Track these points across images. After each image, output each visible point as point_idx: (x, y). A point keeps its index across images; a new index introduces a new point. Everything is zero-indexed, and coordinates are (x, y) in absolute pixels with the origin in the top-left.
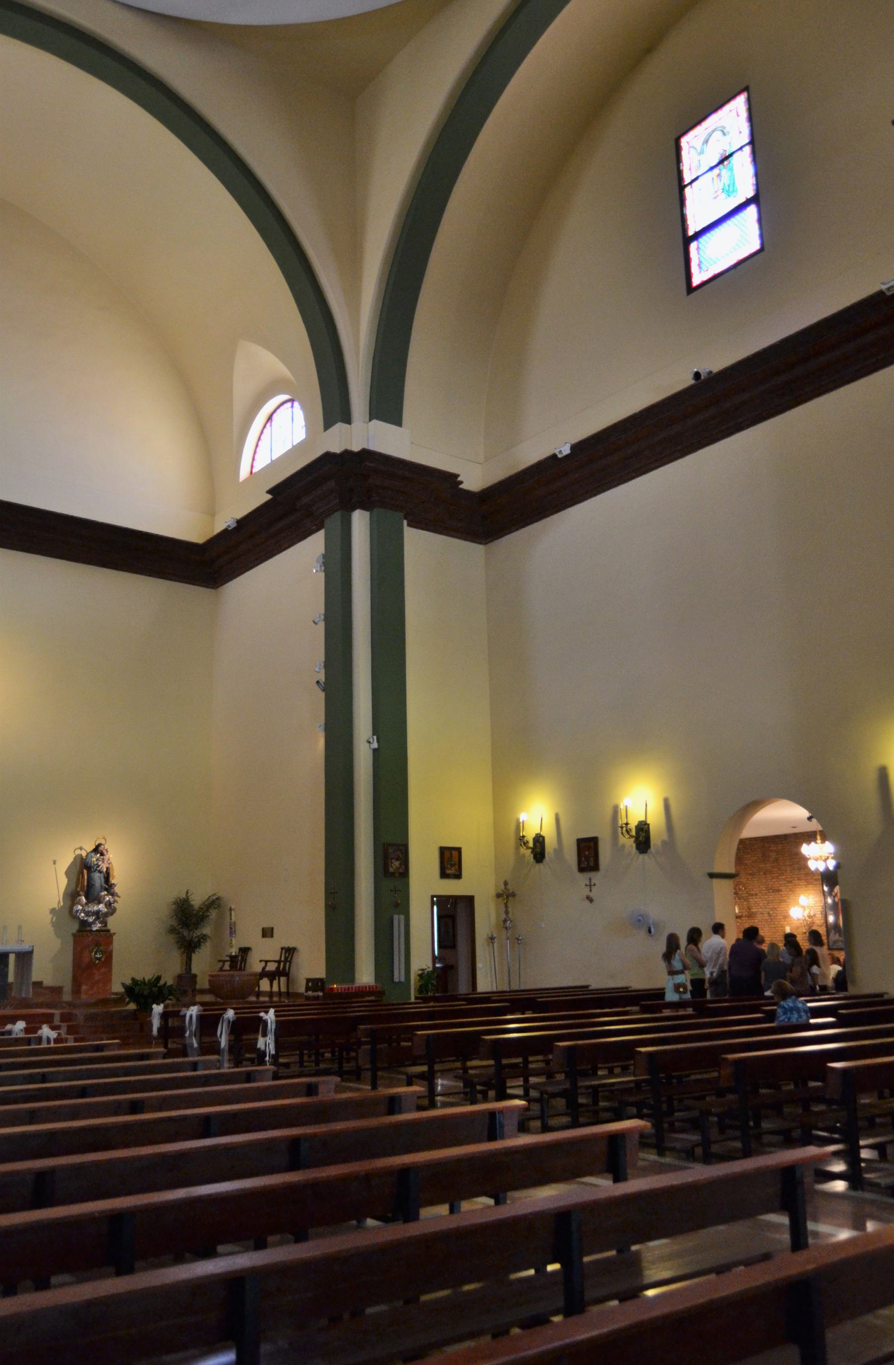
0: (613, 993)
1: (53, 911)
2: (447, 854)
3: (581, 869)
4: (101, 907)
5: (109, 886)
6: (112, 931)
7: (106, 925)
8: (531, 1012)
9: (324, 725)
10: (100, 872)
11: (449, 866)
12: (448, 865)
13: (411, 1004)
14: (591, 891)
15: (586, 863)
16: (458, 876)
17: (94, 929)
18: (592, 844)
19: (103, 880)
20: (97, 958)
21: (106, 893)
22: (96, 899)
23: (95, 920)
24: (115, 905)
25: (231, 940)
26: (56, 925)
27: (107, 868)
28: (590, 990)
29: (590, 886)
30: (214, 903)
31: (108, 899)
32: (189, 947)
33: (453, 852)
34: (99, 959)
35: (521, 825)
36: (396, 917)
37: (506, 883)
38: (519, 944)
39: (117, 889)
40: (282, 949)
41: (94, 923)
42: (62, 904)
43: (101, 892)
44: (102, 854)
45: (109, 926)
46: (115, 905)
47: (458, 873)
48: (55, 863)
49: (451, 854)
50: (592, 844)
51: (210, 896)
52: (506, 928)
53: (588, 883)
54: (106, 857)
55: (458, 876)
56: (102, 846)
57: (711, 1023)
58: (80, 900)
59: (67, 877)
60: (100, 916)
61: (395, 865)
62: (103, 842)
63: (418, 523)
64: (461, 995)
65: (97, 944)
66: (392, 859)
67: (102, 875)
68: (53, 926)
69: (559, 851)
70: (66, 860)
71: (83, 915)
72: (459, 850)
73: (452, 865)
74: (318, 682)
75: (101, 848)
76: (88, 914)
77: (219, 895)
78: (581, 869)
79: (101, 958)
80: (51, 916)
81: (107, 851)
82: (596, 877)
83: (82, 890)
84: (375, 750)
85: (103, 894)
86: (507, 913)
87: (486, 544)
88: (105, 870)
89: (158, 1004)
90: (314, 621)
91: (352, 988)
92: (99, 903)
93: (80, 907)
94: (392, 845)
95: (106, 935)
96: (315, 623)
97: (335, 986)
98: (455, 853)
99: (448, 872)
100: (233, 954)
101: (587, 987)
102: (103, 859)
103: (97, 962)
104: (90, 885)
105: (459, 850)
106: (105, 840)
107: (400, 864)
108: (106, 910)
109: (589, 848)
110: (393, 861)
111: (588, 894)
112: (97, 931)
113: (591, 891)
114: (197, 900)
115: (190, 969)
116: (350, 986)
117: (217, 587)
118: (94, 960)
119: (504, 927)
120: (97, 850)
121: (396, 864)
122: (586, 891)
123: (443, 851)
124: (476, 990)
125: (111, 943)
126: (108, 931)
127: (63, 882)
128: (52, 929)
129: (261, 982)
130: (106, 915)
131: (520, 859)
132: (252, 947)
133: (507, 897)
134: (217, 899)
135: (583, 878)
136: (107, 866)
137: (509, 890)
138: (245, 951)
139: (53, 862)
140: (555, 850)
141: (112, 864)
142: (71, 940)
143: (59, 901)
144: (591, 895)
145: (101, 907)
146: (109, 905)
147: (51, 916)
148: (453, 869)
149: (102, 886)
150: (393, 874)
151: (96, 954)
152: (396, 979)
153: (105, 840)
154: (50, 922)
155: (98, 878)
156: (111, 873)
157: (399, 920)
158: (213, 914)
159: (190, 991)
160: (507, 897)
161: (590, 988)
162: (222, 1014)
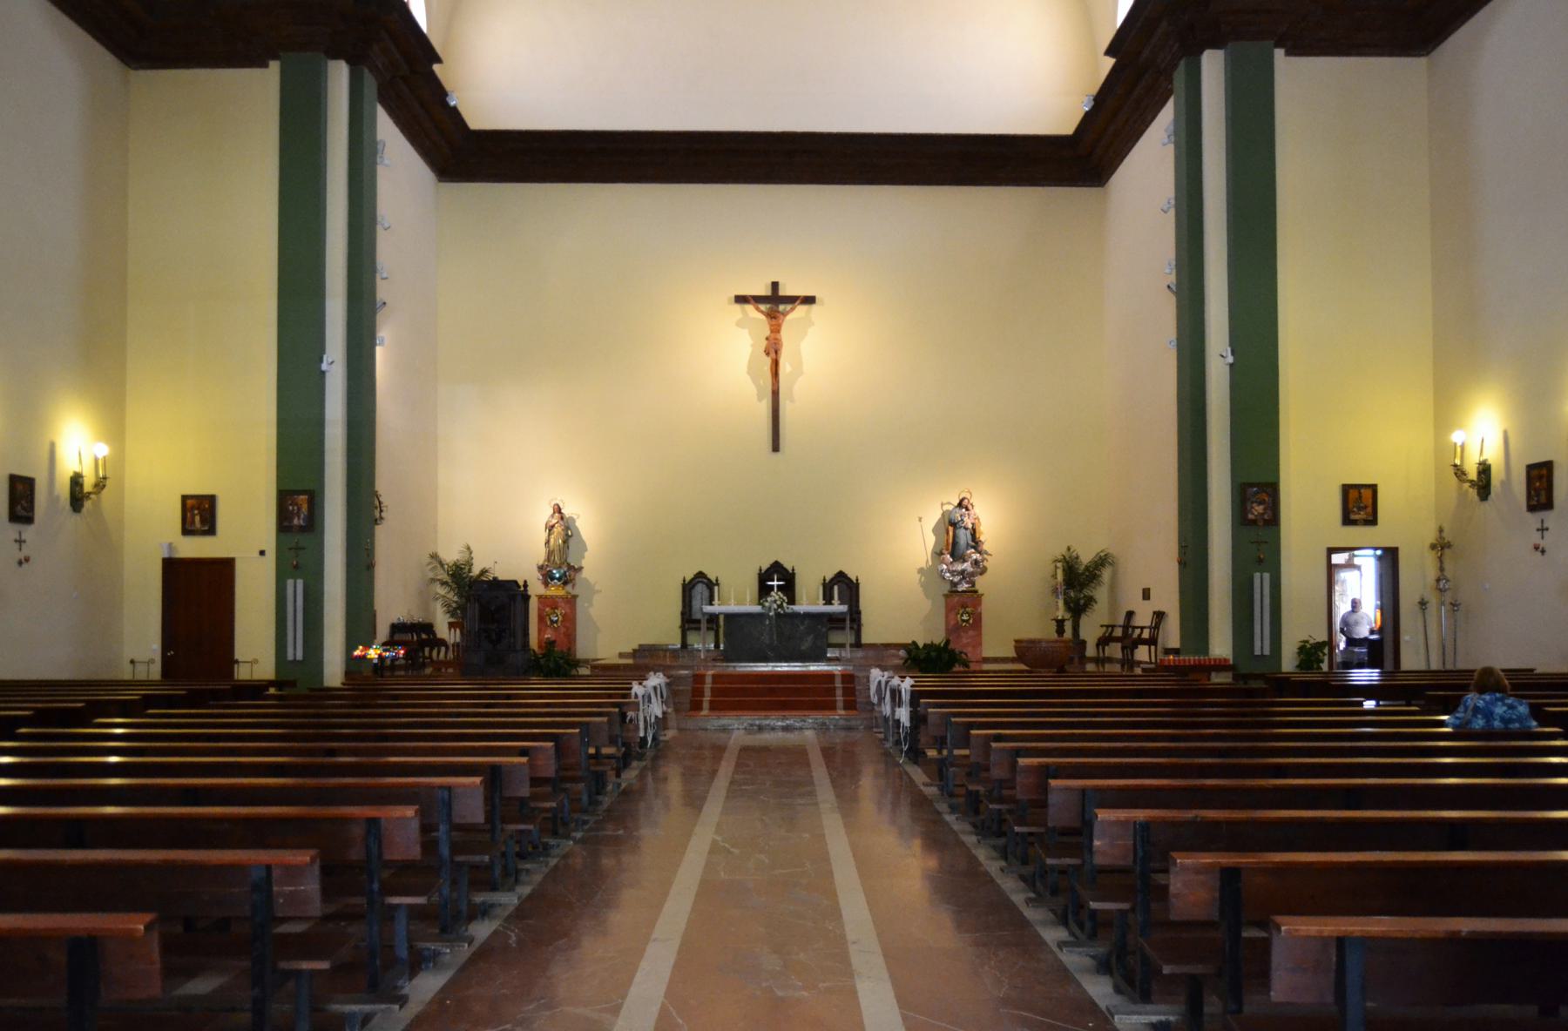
0: (1547, 679)
1: (921, 571)
2: (1353, 494)
3: (1532, 508)
4: (967, 566)
5: (976, 543)
6: (980, 592)
7: (973, 585)
8: (1404, 703)
9: (1175, 341)
10: (966, 529)
11: (1355, 509)
12: (1354, 507)
13: (1135, 676)
14: (1543, 538)
15: (1536, 499)
16: (1372, 521)
17: (960, 589)
18: (1544, 472)
19: (969, 537)
20: (964, 621)
21: (973, 550)
22: (961, 558)
23: (961, 580)
24: (985, 563)
25: (1057, 602)
26: (924, 586)
27: (973, 524)
28: (1536, 675)
29: (1543, 530)
30: (1102, 561)
31: (975, 557)
32: (1078, 608)
33: (1362, 491)
34: (967, 621)
35: (1459, 450)
36: (1257, 575)
37: (1441, 530)
38: (1454, 611)
39: (985, 547)
40: (1154, 613)
41: (959, 582)
42: (930, 563)
43: (967, 549)
44: (967, 509)
45: (978, 587)
46: (985, 563)
47: (1371, 518)
48: (920, 519)
49: (1360, 493)
50: (1544, 472)
51: (548, 542)
52: (1440, 590)
53: (1540, 527)
54: (972, 512)
55: (1372, 521)
56: (966, 501)
57: (973, 703)
58: (943, 559)
59: (935, 534)
60: (965, 575)
61: (1256, 510)
62: (968, 496)
63: (1297, 48)
64: (986, 660)
65: (964, 606)
66: (1253, 502)
67: (968, 532)
68: (922, 586)
69: (1507, 483)
70: (933, 516)
71: (948, 575)
72: (1373, 488)
73: (1360, 509)
74: (1169, 287)
75: (965, 502)
76: (953, 573)
77: (1108, 551)
78: (1532, 508)
79: (969, 620)
80: (919, 575)
81: (973, 506)
82: (1550, 518)
83: (947, 549)
84: (1231, 365)
85: (969, 552)
86: (1442, 569)
87: (1428, 54)
88: (970, 526)
89: (404, 654)
90: (1162, 210)
91: (1189, 660)
92: (964, 561)
93: (945, 567)
94: (1252, 485)
95: (974, 596)
96: (1165, 212)
97: (1171, 657)
98: (1367, 494)
99: (1353, 517)
100: (1060, 618)
101: (1532, 670)
102: (969, 515)
103: (964, 624)
104: (955, 543)
105: (1373, 488)
106: (971, 494)
107: (1265, 509)
108: (972, 569)
109: (1540, 478)
110: (1254, 505)
111: (1538, 542)
112: (963, 591)
113: (1543, 538)
114: (1086, 557)
115: (1078, 635)
116: (1187, 658)
117: (1105, 184)
118: (960, 622)
119: (1437, 588)
120: (960, 505)
121: (1259, 509)
122: (1536, 538)
123: (14, 480)
124: (1399, 668)
125: (979, 603)
126: (976, 592)
127: (931, 540)
128: (921, 589)
129: (1140, 647)
130: (972, 574)
131: (1462, 496)
132: (1135, 611)
133: (1442, 548)
134: (1106, 555)
135: (1533, 520)
136: (973, 521)
137: (1444, 539)
138: (1130, 614)
139: (917, 519)
140: (1502, 483)
141: (979, 520)
142: (942, 601)
143: (927, 561)
144: (1542, 544)
145: (967, 566)
146: (976, 562)
147: (919, 575)
148: (1362, 513)
149: (968, 544)
150: (1254, 522)
151: (962, 615)
152: (1257, 652)
153: (971, 494)
154: (918, 581)
155: (964, 537)
156: (977, 528)
157: (1261, 581)
158: (1106, 574)
159: (1076, 660)
160: (1442, 548)
161: (1535, 672)
162: (1460, 697)
